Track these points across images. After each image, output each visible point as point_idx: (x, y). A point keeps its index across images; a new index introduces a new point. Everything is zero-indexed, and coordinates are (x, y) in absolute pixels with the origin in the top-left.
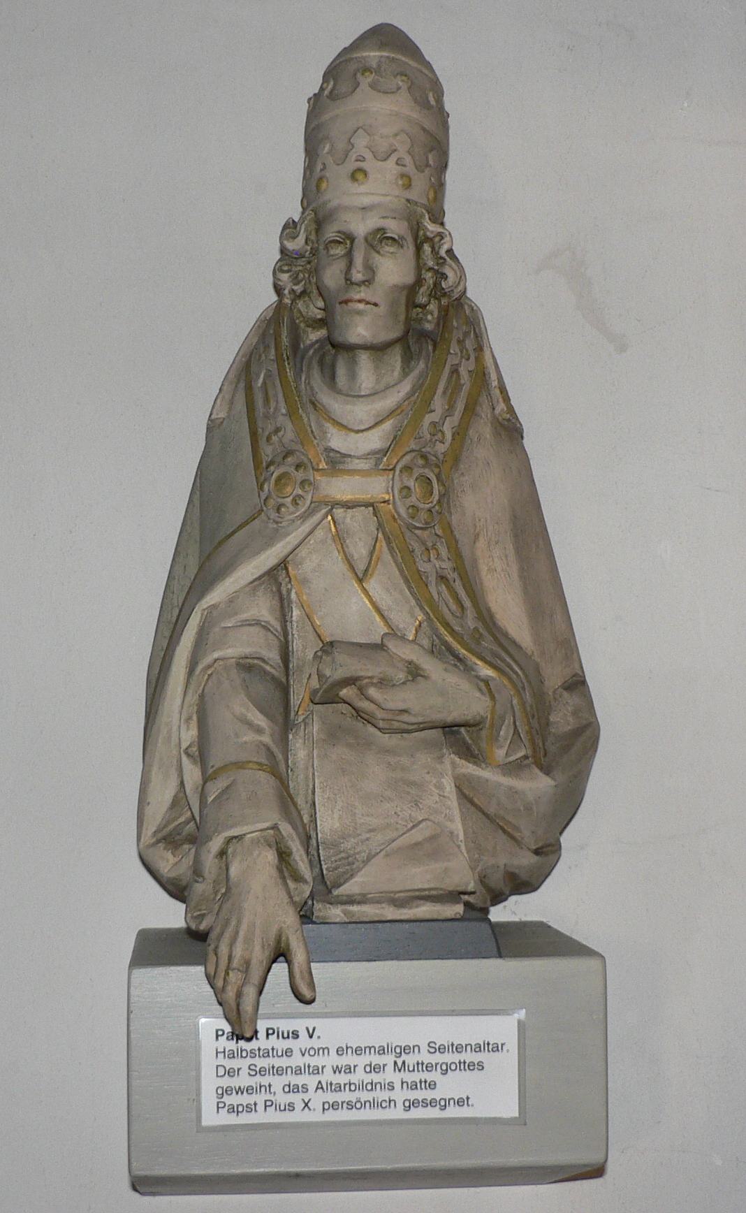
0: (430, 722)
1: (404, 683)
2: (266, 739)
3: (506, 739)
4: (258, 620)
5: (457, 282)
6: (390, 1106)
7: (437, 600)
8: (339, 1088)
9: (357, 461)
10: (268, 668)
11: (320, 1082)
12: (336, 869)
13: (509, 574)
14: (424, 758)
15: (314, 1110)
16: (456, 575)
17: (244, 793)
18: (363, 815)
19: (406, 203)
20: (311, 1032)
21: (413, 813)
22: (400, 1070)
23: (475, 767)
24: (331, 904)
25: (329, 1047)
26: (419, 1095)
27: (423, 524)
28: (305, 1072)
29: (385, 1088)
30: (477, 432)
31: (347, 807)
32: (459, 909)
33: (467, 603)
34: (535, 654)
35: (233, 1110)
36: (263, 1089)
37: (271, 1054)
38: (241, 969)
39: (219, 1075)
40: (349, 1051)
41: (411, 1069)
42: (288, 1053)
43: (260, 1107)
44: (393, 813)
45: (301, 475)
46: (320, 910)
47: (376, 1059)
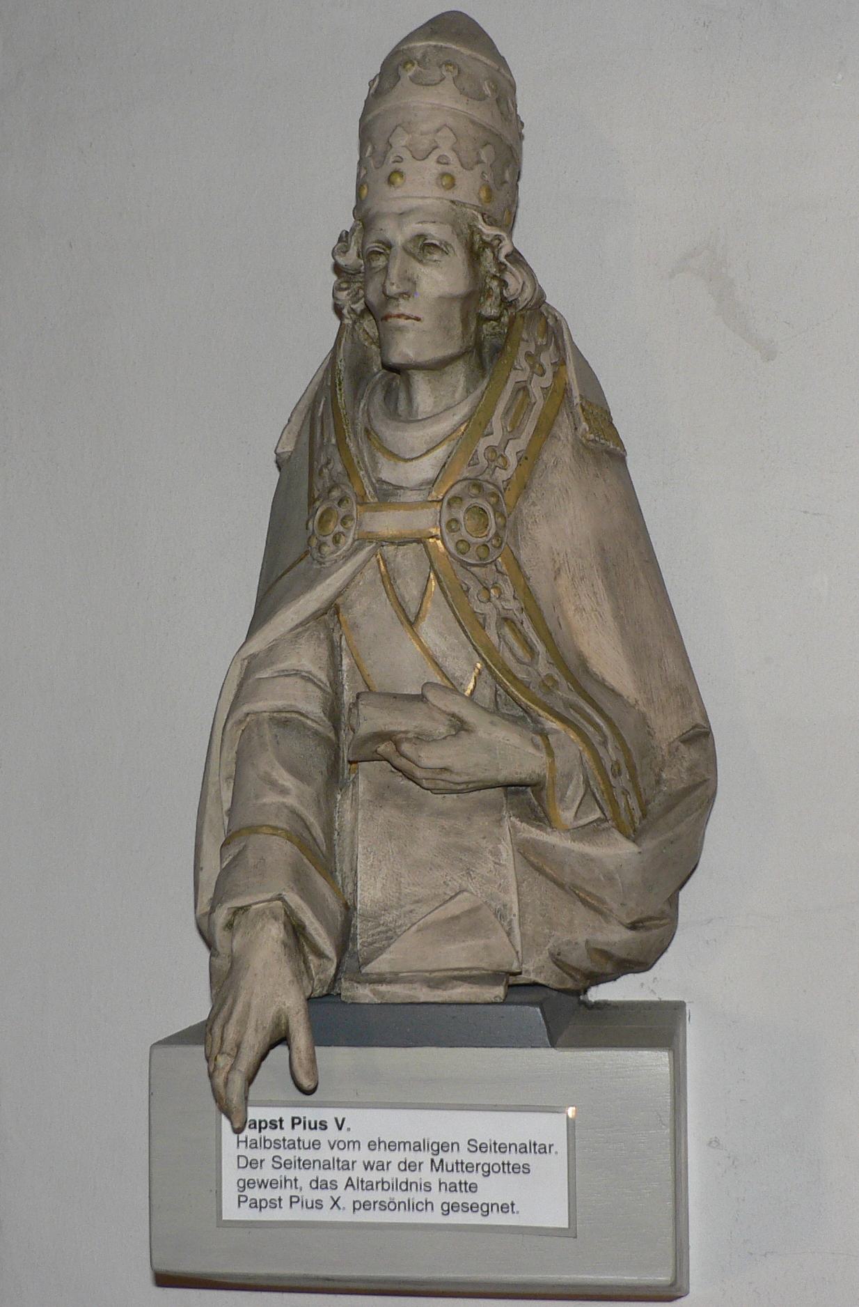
0: (479, 781)
1: (445, 738)
2: (291, 801)
3: (574, 801)
4: (298, 671)
5: (520, 290)
6: (426, 1208)
7: (497, 645)
8: (370, 1186)
9: (409, 493)
10: (309, 722)
11: (350, 1179)
12: (371, 944)
13: (599, 613)
14: (483, 821)
15: (344, 1208)
16: (524, 616)
17: (252, 860)
18: (409, 884)
19: (450, 204)
20: (340, 1123)
21: (464, 883)
22: (437, 1170)
23: (538, 831)
24: (359, 983)
25: (360, 1141)
26: (459, 1198)
27: (477, 560)
28: (334, 1167)
29: (421, 1189)
30: (553, 456)
31: (392, 875)
32: (499, 991)
33: (540, 647)
34: (640, 702)
35: (255, 1204)
36: (288, 1183)
37: (297, 1146)
38: (231, 1053)
39: (241, 1165)
40: (382, 1145)
41: (450, 1169)
42: (315, 1145)
43: (285, 1203)
44: (442, 883)
45: (343, 510)
46: (347, 989)
47: (411, 1156)
